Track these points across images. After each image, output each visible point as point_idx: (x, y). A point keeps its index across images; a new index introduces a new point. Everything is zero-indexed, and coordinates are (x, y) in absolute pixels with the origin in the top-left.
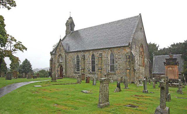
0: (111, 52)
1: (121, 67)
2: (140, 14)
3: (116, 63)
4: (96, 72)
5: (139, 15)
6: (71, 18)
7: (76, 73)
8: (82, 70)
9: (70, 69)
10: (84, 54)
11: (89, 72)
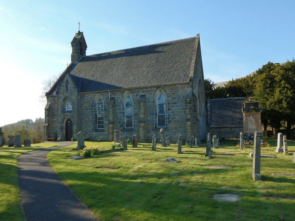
0: (159, 92)
1: (177, 118)
2: (197, 35)
3: (169, 111)
4: (133, 127)
5: (196, 36)
6: (80, 33)
7: (97, 131)
8: (111, 126)
9: (87, 124)
10: (113, 96)
11: (122, 128)
